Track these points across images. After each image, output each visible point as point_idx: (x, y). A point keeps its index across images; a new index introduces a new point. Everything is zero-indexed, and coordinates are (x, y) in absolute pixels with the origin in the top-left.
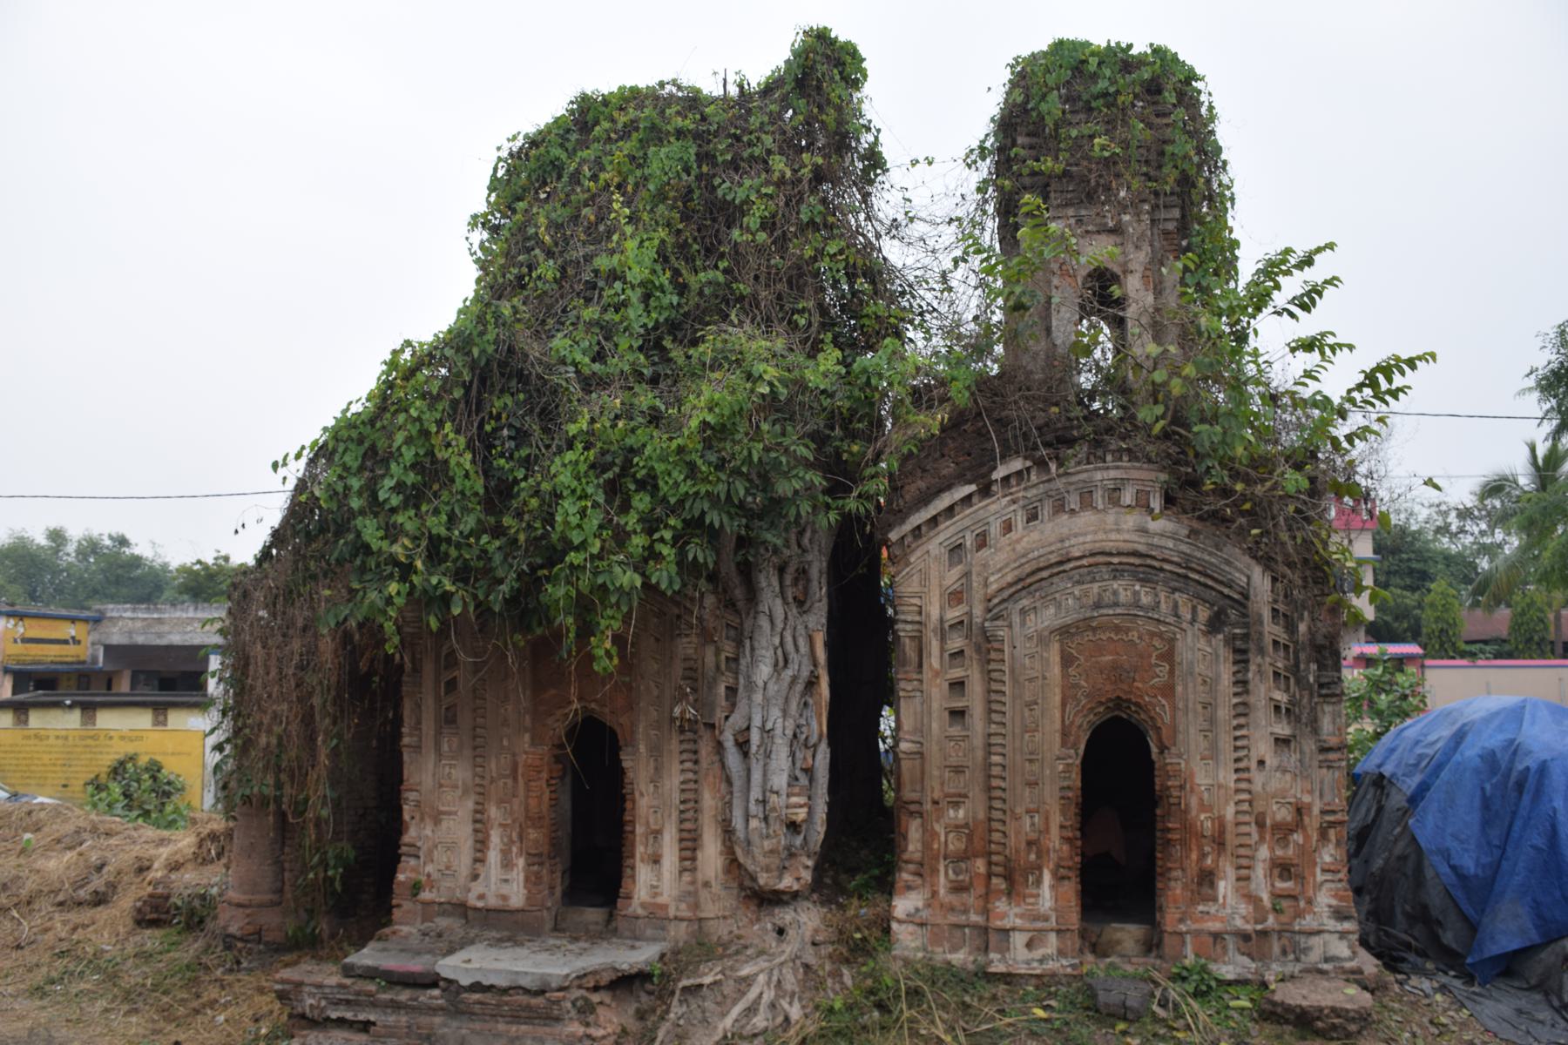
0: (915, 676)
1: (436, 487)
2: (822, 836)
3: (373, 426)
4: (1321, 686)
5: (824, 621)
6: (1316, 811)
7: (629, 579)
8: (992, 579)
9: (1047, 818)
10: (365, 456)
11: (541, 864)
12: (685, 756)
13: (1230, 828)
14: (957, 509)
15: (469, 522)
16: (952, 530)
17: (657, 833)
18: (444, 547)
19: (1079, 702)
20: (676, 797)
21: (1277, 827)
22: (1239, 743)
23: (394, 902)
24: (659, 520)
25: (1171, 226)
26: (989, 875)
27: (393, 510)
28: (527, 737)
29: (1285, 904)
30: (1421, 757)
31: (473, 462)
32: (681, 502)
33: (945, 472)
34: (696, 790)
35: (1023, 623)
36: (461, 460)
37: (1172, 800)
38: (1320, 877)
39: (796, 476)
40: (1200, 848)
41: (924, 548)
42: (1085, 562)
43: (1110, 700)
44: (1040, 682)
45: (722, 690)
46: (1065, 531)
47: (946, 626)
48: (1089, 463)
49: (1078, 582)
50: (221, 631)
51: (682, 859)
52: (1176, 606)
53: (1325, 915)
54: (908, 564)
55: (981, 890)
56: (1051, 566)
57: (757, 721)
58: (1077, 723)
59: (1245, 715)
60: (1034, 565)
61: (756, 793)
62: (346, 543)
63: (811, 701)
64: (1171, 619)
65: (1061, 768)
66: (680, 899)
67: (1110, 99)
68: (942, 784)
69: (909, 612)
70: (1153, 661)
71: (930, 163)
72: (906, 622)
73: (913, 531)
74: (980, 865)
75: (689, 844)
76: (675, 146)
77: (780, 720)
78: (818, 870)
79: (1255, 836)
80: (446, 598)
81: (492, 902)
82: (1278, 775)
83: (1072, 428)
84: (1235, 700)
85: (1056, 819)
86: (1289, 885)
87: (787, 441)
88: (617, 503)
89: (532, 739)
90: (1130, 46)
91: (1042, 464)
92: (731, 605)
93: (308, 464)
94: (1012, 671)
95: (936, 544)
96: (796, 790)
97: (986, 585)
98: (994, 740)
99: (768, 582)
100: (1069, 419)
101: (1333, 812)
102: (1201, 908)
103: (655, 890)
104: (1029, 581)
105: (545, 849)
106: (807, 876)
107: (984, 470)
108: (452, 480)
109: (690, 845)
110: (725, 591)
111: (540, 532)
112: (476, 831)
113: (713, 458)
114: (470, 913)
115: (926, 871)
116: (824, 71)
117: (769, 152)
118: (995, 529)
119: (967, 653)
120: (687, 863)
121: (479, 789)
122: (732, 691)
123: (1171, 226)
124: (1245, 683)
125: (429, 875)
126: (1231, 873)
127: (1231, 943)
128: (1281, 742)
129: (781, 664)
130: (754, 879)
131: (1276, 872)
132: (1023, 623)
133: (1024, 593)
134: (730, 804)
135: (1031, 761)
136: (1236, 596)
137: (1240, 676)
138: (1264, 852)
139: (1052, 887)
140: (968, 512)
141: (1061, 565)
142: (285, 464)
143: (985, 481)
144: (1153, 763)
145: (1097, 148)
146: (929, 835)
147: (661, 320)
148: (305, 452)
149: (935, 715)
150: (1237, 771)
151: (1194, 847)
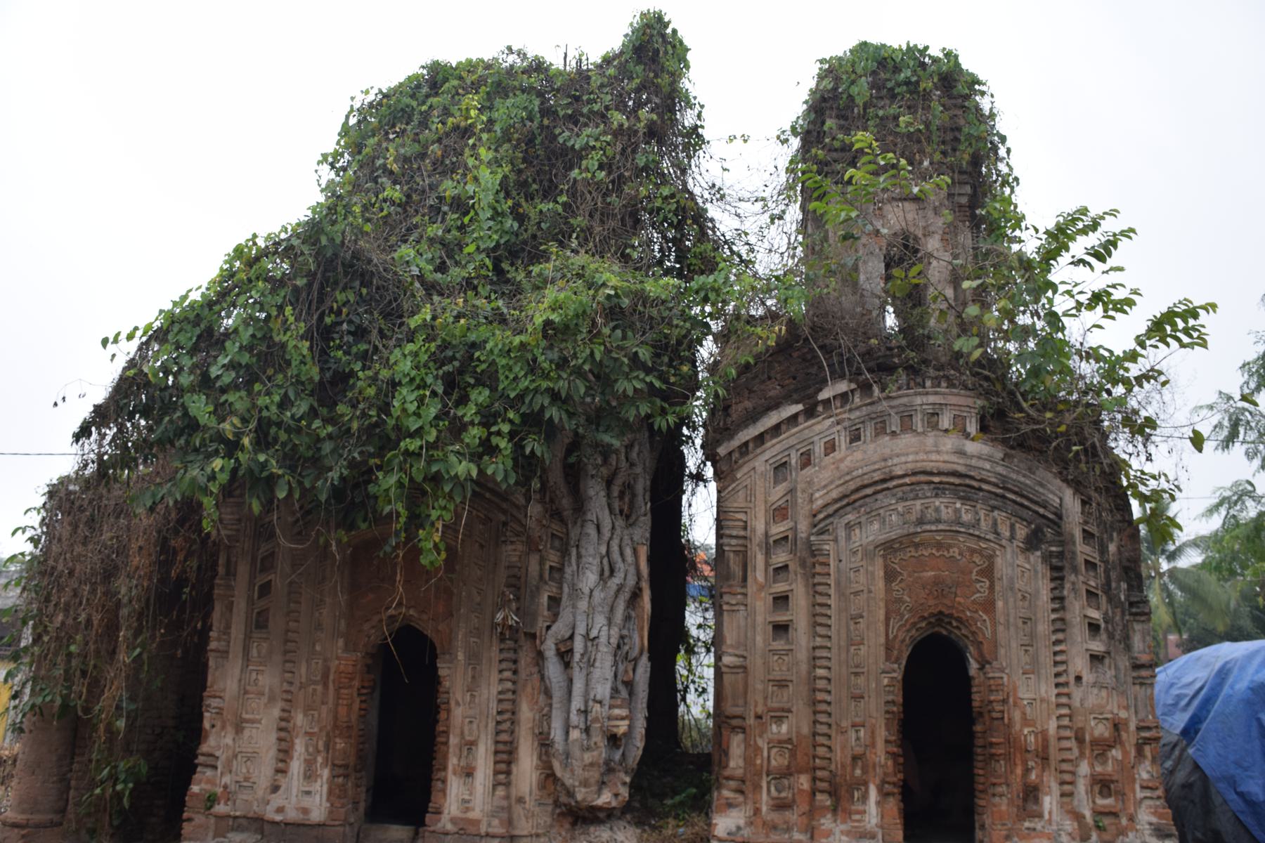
0: (739, 590)
1: (270, 372)
2: (640, 752)
3: (211, 309)
5: (648, 535)
6: (1132, 726)
7: (463, 468)
8: (817, 495)
9: (873, 732)
10: (199, 337)
11: (346, 776)
12: (504, 665)
13: (1052, 741)
14: (784, 427)
15: (302, 407)
16: (778, 448)
17: (471, 745)
18: (273, 430)
19: (902, 616)
20: (494, 707)
21: (1095, 742)
22: (1058, 658)
23: (185, 815)
24: (496, 415)
25: (964, 200)
26: (813, 793)
27: (223, 390)
28: (341, 642)
29: (1106, 821)
30: (1179, 697)
31: (311, 349)
32: (521, 397)
33: (772, 393)
34: (514, 701)
35: (848, 538)
36: (298, 347)
37: (995, 715)
38: (1140, 794)
39: (637, 377)
40: (1025, 762)
41: (751, 465)
42: (907, 480)
43: (932, 615)
44: (865, 596)
45: (544, 599)
46: (887, 451)
47: (771, 540)
48: (908, 388)
49: (903, 499)
50: (31, 539)
51: (496, 773)
52: (995, 523)
53: (1147, 832)
54: (734, 480)
55: (805, 807)
56: (875, 483)
57: (581, 629)
58: (900, 637)
59: (1063, 631)
60: (859, 483)
61: (577, 703)
62: (171, 421)
63: (633, 614)
64: (991, 536)
65: (886, 681)
66: (493, 815)
67: (912, 88)
68: (766, 698)
69: (734, 527)
70: (974, 577)
71: (745, 141)
72: (731, 537)
73: (740, 447)
74: (804, 782)
75: (505, 757)
76: (521, 98)
77: (605, 628)
78: (634, 787)
79: (1076, 752)
80: (272, 481)
81: (292, 815)
82: (1095, 691)
83: (892, 356)
84: (1054, 616)
85: (882, 734)
86: (1109, 801)
87: (627, 344)
88: (455, 397)
89: (346, 644)
90: (926, 48)
91: (866, 388)
92: (556, 515)
93: (140, 349)
94: (838, 583)
96: (619, 702)
97: (811, 501)
98: (819, 653)
99: (595, 493)
100: (890, 349)
101: (1149, 728)
102: (1027, 824)
103: (466, 804)
104: (853, 497)
105: (352, 761)
106: (625, 792)
107: (811, 391)
108: (288, 363)
109: (505, 757)
110: (552, 501)
111: (375, 419)
112: (280, 740)
113: (555, 355)
114: (266, 827)
115: (748, 787)
116: (653, 53)
117: (607, 108)
118: (819, 449)
119: (792, 567)
120: (502, 777)
121: (285, 696)
122: (555, 601)
123: (964, 200)
124: (1061, 599)
125: (225, 787)
126: (1055, 786)
128: (1096, 659)
129: (607, 573)
130: (570, 794)
131: (1097, 788)
132: (848, 538)
133: (849, 509)
134: (548, 716)
135: (856, 674)
136: (1051, 516)
137: (1057, 593)
138: (1084, 768)
139: (878, 803)
140: (796, 430)
141: (885, 483)
142: (116, 341)
143: (811, 401)
144: (968, 680)
145: (902, 125)
146: (752, 752)
147: (502, 241)
148: (139, 333)
149: (759, 629)
150: (1057, 685)
151: (1018, 762)
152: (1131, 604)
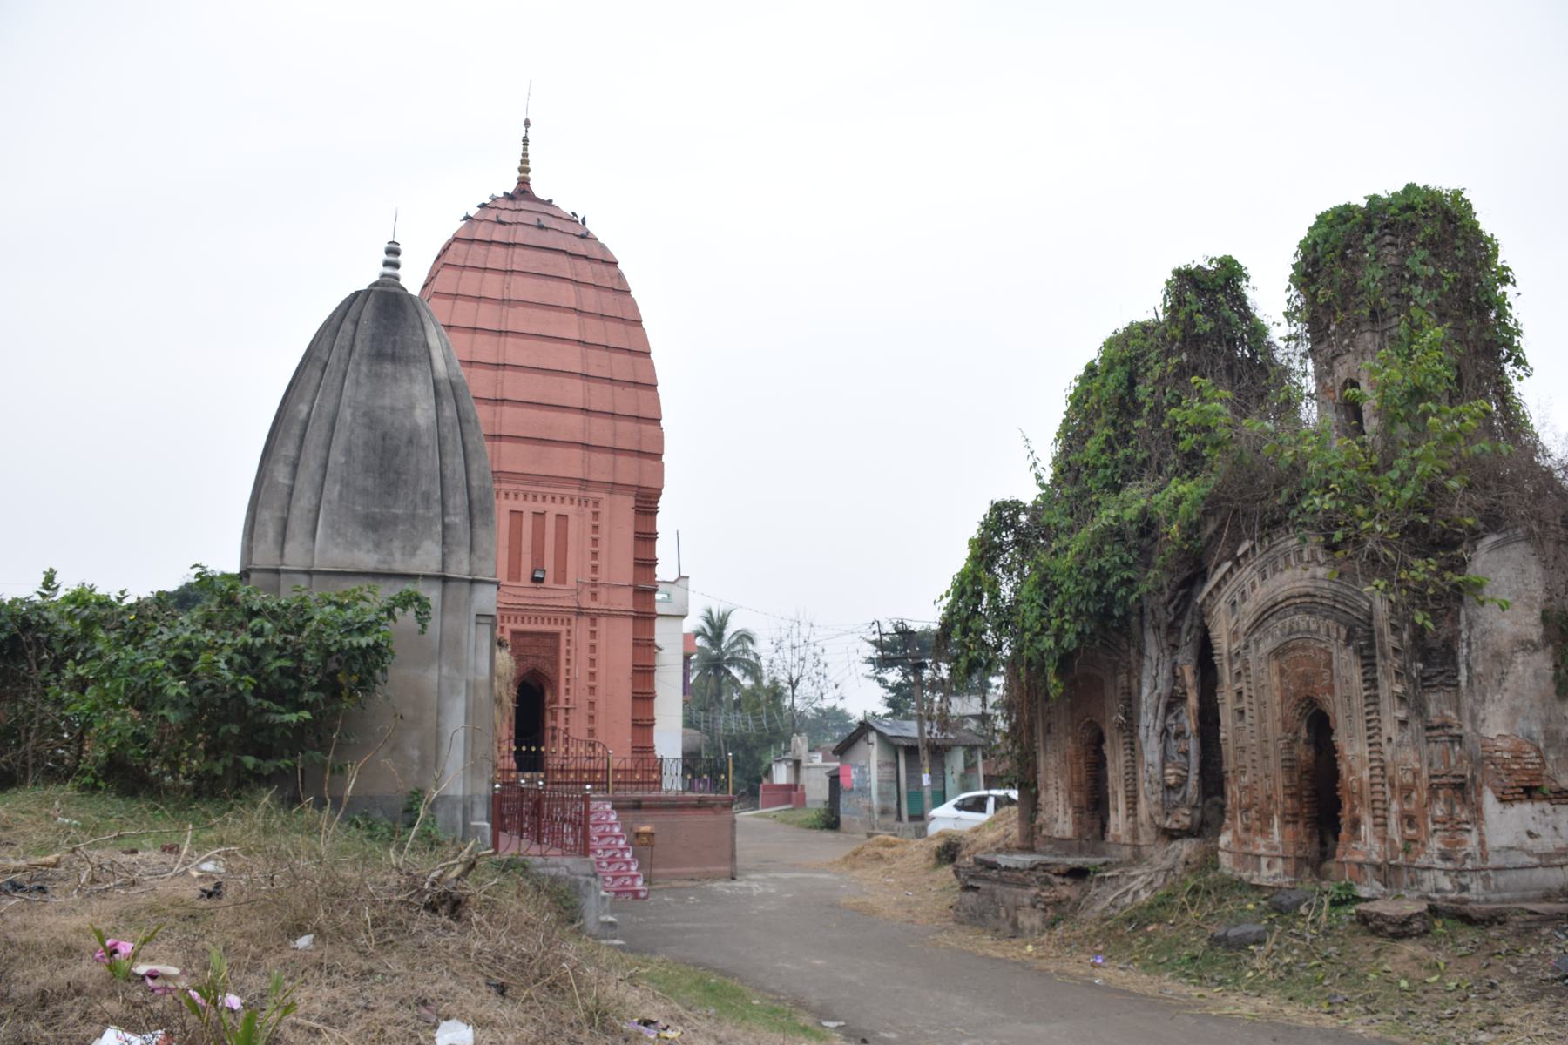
38: (1431, 827)
59: (1375, 704)
79: (1389, 795)
95: (1223, 604)
118: (1247, 588)
124: (1374, 681)
127: (1369, 871)
128: (1403, 723)
132: (1257, 649)
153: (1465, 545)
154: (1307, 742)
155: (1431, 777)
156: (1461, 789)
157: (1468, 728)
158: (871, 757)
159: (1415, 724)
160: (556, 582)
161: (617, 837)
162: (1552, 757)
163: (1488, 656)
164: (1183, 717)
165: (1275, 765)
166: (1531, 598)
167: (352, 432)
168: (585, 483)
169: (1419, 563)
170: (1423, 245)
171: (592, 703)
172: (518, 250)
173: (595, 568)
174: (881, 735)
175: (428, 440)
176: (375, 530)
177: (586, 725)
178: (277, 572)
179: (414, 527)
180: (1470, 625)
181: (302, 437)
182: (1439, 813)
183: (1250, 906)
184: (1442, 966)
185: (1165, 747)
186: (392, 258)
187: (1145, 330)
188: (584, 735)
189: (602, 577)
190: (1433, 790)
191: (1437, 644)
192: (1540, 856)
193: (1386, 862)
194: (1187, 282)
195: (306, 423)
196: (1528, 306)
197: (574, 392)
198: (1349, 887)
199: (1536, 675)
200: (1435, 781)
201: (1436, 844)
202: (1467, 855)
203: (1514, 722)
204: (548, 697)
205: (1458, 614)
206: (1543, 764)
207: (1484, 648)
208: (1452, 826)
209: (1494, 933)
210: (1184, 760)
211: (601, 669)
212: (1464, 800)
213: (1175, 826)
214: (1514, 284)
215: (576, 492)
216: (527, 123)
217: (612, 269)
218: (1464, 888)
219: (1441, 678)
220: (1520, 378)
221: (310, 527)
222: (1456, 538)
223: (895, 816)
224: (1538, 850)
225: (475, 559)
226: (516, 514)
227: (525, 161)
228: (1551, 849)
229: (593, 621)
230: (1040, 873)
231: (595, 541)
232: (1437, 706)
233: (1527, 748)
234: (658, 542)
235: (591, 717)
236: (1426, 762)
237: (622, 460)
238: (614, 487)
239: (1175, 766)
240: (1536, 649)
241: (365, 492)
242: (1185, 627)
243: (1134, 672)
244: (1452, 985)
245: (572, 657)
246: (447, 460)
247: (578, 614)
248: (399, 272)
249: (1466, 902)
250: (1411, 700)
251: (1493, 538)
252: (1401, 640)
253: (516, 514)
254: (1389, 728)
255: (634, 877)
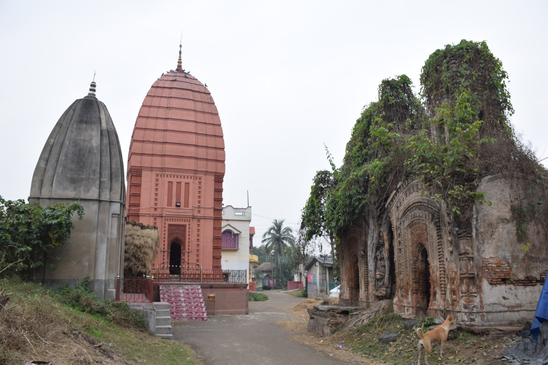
4: (459, 234)
38: (461, 295)
59: (441, 245)
95: (394, 208)
127: (439, 313)
128: (452, 252)
132: (404, 224)
139: (411, 295)
152: (459, 234)
153: (476, 180)
154: (421, 261)
155: (461, 274)
156: (472, 279)
157: (476, 254)
158: (317, 270)
159: (455, 253)
160: (185, 207)
161: (200, 298)
162: (515, 266)
163: (486, 225)
164: (383, 252)
165: (409, 271)
166: (507, 201)
167: (68, 149)
168: (196, 171)
169: (456, 187)
170: (466, 62)
171: (198, 250)
172: (173, 90)
173: (199, 202)
174: (320, 263)
175: (96, 151)
176: (74, 183)
177: (196, 258)
178: (39, 198)
179: (89, 182)
180: (478, 212)
181: (51, 151)
182: (464, 289)
183: (398, 326)
184: (457, 352)
185: (376, 264)
186: (93, 88)
187: (374, 105)
188: (195, 262)
189: (202, 205)
190: (462, 279)
191: (463, 220)
192: (508, 307)
193: (445, 309)
194: (388, 86)
195: (52, 146)
196: (512, 86)
197: (192, 139)
198: (432, 319)
199: (508, 233)
200: (462, 276)
201: (462, 302)
202: (474, 307)
203: (497, 252)
204: (182, 248)
205: (472, 208)
206: (511, 269)
207: (484, 222)
208: (469, 294)
209: (482, 339)
210: (383, 269)
211: (201, 238)
212: (474, 284)
213: (380, 295)
214: (507, 77)
215: (192, 175)
216: (181, 46)
217: (208, 96)
218: (473, 320)
219: (464, 234)
220: (511, 115)
221: (51, 182)
222: (474, 177)
223: (325, 293)
224: (508, 304)
225: (112, 193)
226: (170, 183)
227: (180, 59)
228: (514, 304)
229: (199, 221)
230: (331, 312)
231: (200, 192)
232: (463, 246)
233: (504, 262)
234: (223, 192)
235: (198, 255)
236: (459, 268)
237: (210, 163)
238: (206, 173)
239: (380, 271)
240: (508, 221)
241: (71, 170)
242: (384, 218)
243: (366, 235)
244: (458, 360)
245: (191, 233)
246: (103, 158)
247: (193, 218)
248: (95, 93)
249: (473, 326)
250: (453, 243)
251: (489, 177)
252: (450, 219)
253: (170, 183)
254: (447, 255)
255: (203, 313)
